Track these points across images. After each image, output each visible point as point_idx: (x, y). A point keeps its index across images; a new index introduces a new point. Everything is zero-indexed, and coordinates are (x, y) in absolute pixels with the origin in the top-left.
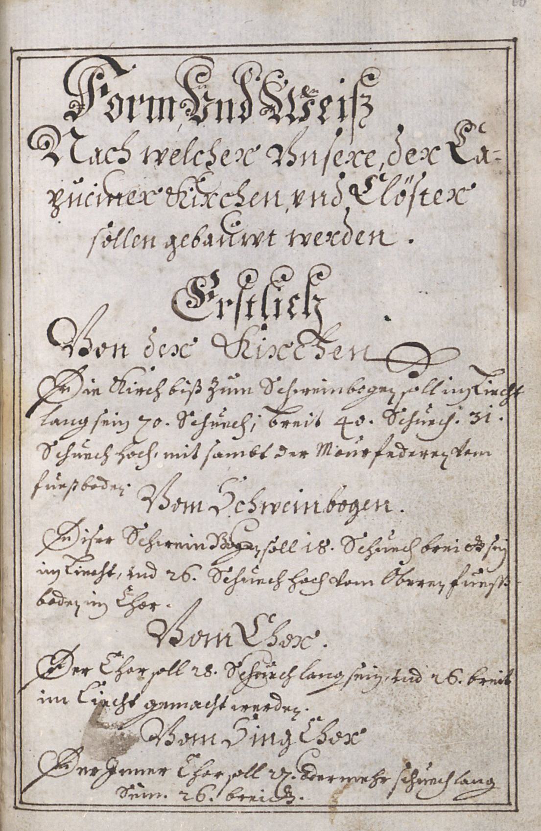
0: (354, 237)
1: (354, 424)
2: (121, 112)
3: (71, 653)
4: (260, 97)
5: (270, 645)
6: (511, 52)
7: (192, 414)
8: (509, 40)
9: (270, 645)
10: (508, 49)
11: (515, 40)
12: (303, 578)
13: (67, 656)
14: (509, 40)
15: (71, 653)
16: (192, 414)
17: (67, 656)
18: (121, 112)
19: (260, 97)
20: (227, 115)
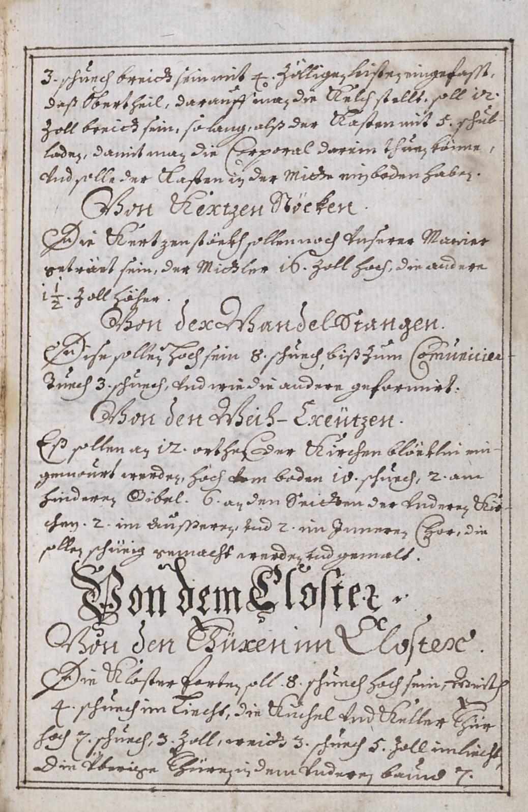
0: (175, 420)
1: (258, 375)
2: (140, 607)
3: (78, 666)
4: (73, 584)
5: (269, 425)
6: (509, 51)
7: (301, 495)
8: (506, 41)
9: (269, 425)
10: (506, 49)
11: (512, 41)
12: (438, 172)
13: (74, 669)
14: (506, 41)
15: (78, 666)
16: (301, 495)
17: (74, 669)
18: (140, 607)
19: (73, 584)
20: (158, 609)
